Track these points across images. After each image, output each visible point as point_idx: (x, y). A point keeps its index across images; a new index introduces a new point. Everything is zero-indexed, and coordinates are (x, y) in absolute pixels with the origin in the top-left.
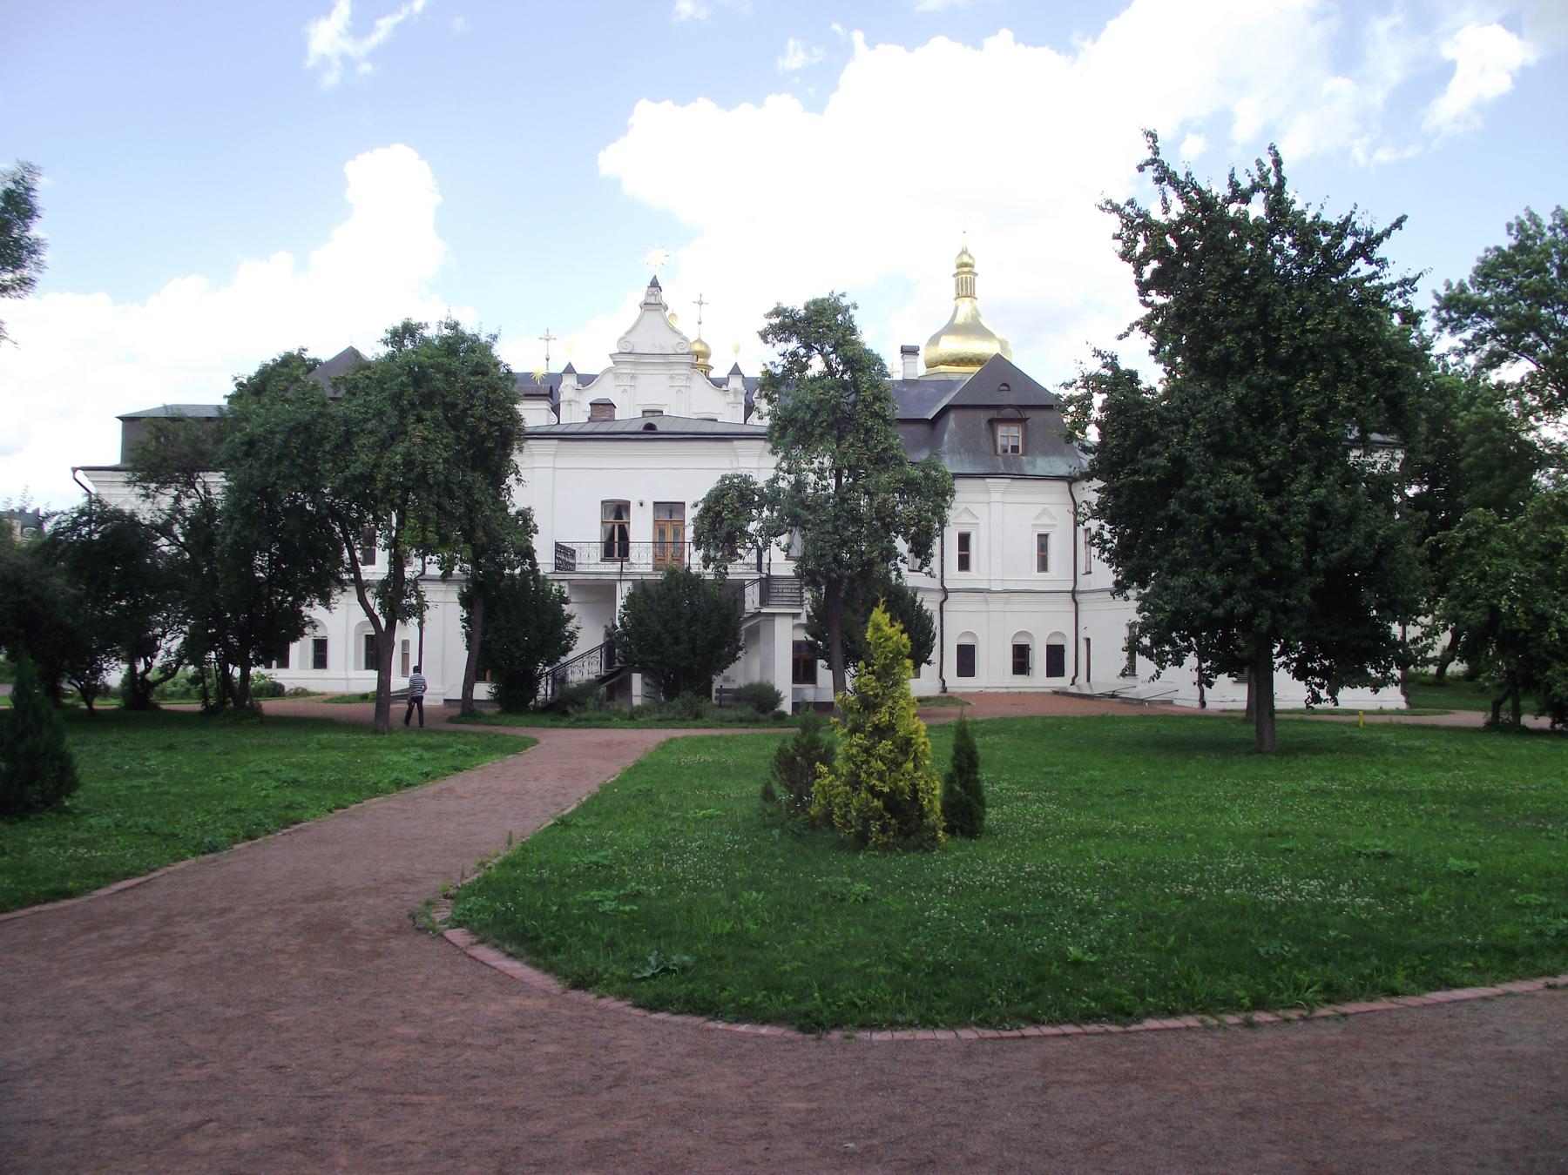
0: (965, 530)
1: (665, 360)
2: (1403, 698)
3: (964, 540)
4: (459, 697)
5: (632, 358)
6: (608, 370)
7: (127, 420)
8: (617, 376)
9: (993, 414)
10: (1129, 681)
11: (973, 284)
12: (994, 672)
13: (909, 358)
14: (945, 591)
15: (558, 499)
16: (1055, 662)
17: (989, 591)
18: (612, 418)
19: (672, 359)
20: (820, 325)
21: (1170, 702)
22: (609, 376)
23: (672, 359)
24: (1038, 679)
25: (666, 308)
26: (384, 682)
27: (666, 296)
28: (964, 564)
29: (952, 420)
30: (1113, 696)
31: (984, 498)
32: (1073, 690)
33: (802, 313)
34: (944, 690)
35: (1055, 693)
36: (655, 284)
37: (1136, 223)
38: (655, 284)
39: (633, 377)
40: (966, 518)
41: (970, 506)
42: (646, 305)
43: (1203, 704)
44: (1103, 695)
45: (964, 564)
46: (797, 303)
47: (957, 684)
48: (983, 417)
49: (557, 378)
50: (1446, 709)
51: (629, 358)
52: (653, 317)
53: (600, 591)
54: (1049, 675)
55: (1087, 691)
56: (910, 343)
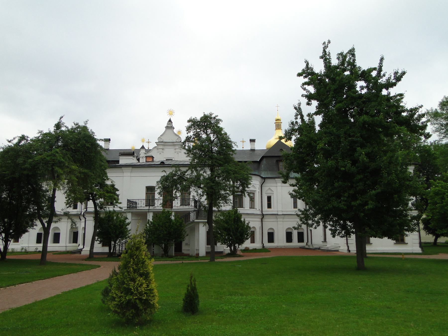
0: (269, 195)
1: (173, 144)
2: (420, 249)
3: (269, 198)
4: (94, 252)
5: (163, 143)
6: (155, 147)
7: (146, 187)
8: (158, 149)
9: (278, 159)
10: (325, 244)
11: (280, 125)
12: (280, 240)
13: (252, 143)
14: (263, 215)
15: (131, 187)
16: (301, 238)
17: (277, 215)
18: (153, 161)
19: (175, 144)
20: (207, 123)
21: (338, 251)
22: (156, 149)
23: (175, 144)
24: (295, 243)
25: (174, 128)
26: (45, 247)
27: (174, 125)
28: (269, 206)
29: (264, 161)
30: (319, 249)
31: (275, 185)
32: (307, 247)
33: (223, 132)
34: (263, 246)
35: (300, 248)
36: (170, 121)
37: (308, 72)
38: (170, 121)
39: (163, 149)
40: (269, 191)
41: (270, 188)
42: (167, 127)
43: (349, 251)
44: (316, 249)
45: (269, 206)
46: (198, 116)
47: (268, 245)
48: (274, 160)
49: (139, 151)
50: (436, 253)
51: (162, 144)
52: (169, 131)
53: (142, 215)
54: (298, 242)
55: (311, 247)
56: (252, 138)
